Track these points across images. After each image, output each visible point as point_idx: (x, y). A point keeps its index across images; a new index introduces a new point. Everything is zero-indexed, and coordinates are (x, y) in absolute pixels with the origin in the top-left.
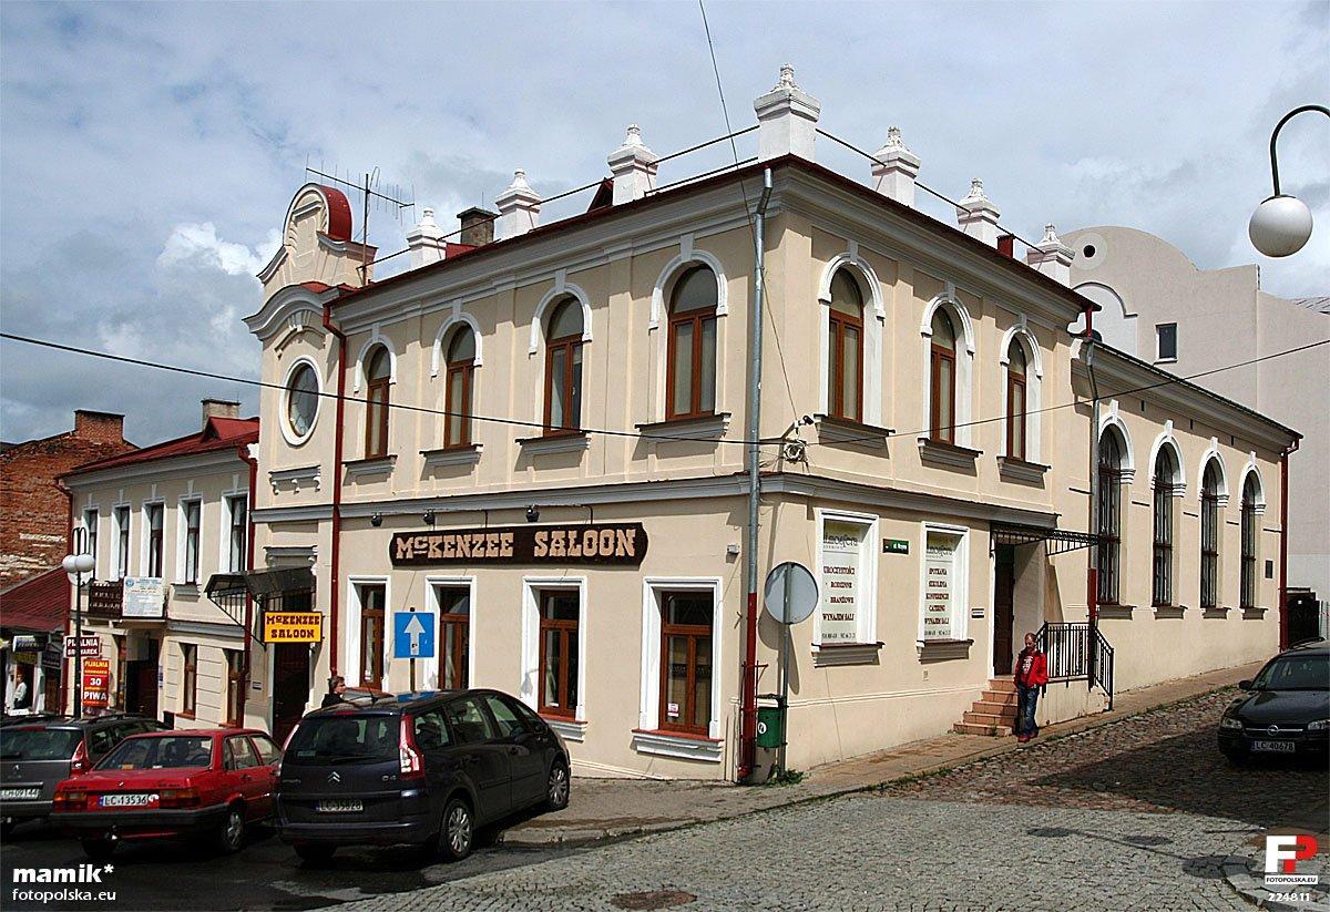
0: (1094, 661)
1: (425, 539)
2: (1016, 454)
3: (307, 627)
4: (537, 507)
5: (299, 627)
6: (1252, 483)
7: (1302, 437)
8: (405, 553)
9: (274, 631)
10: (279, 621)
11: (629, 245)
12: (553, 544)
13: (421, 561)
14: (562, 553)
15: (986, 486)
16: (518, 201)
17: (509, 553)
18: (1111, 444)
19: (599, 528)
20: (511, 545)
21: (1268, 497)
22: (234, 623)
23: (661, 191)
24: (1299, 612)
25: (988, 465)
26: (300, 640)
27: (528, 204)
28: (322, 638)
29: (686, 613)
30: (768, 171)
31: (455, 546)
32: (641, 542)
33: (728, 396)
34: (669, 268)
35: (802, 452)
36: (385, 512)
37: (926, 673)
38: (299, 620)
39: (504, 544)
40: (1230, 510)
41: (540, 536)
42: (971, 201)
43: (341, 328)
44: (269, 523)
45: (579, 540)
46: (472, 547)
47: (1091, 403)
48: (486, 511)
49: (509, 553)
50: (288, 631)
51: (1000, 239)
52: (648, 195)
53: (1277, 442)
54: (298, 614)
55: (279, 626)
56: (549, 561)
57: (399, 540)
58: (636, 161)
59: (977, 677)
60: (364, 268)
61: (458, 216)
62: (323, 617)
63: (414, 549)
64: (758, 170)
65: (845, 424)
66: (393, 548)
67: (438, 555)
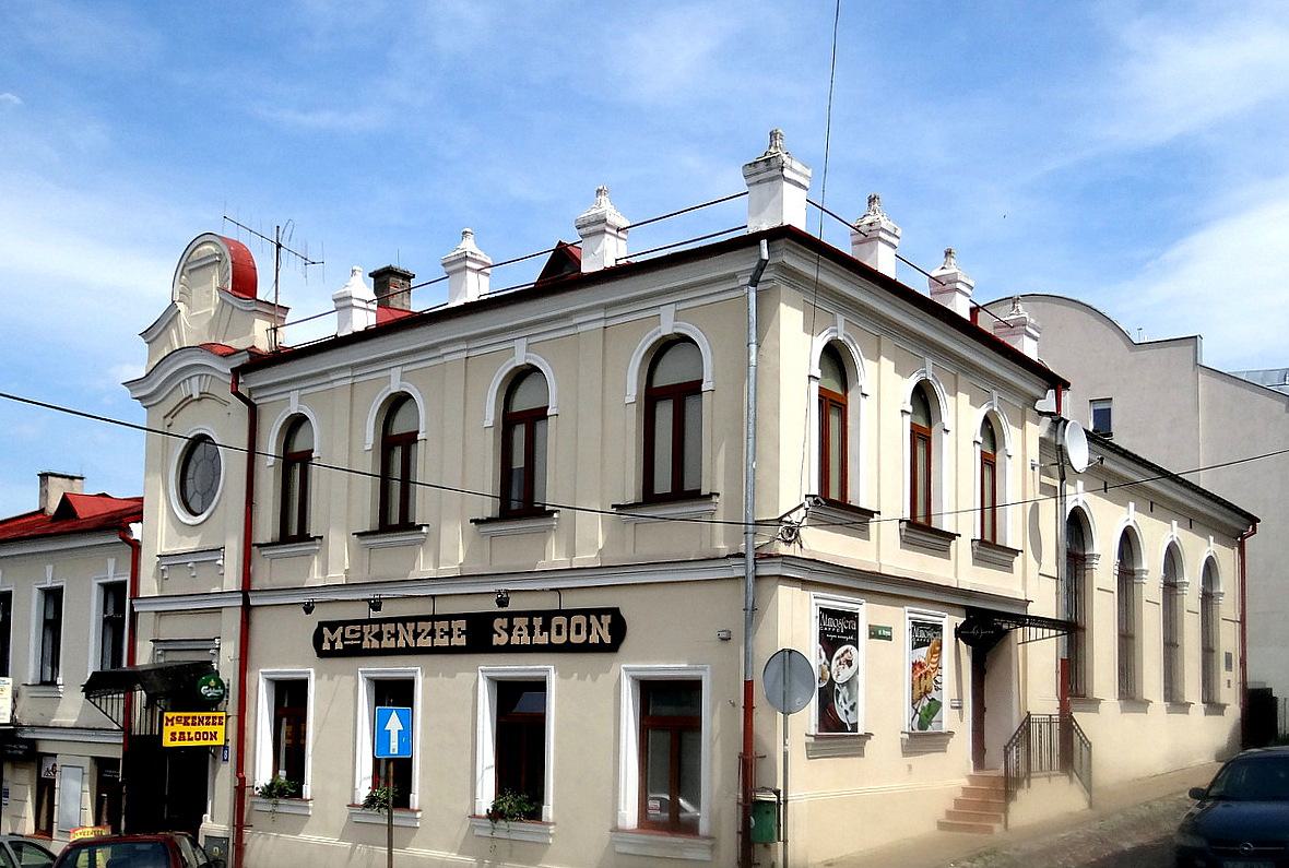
0: (1070, 750)
1: (358, 628)
2: (988, 538)
3: (211, 729)
4: (507, 592)
5: (202, 729)
6: (1210, 567)
7: (1259, 521)
8: (332, 644)
9: (173, 734)
10: (179, 722)
11: (602, 315)
12: (515, 632)
13: (353, 651)
14: (526, 640)
15: (960, 569)
16: (469, 264)
17: (462, 641)
18: (1077, 525)
19: (569, 614)
20: (463, 633)
21: (1227, 583)
22: (116, 727)
23: (633, 260)
24: (1259, 707)
25: (963, 548)
26: (202, 743)
27: (479, 266)
28: (227, 740)
29: (669, 711)
30: (764, 243)
31: (396, 635)
32: (619, 628)
33: (714, 471)
34: (651, 337)
35: (797, 535)
36: (317, 598)
37: (910, 767)
38: (201, 721)
39: (456, 632)
40: (1191, 598)
41: (499, 623)
42: (944, 272)
43: (250, 394)
44: (156, 612)
45: (546, 627)
46: (416, 635)
47: (1058, 483)
48: (433, 597)
49: (462, 641)
50: (189, 733)
51: (972, 310)
52: (620, 262)
53: (1235, 525)
54: (201, 714)
55: (179, 728)
56: (509, 649)
57: (325, 629)
58: (608, 225)
59: (952, 770)
60: (275, 330)
61: (371, 275)
62: (227, 717)
63: (343, 639)
64: (752, 240)
65: (837, 506)
66: (318, 639)
67: (375, 644)
